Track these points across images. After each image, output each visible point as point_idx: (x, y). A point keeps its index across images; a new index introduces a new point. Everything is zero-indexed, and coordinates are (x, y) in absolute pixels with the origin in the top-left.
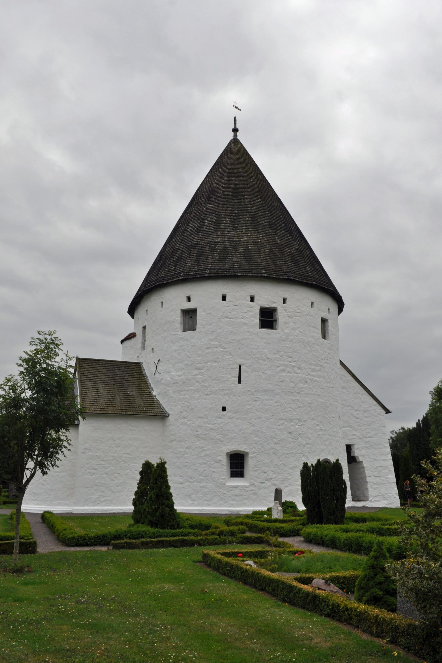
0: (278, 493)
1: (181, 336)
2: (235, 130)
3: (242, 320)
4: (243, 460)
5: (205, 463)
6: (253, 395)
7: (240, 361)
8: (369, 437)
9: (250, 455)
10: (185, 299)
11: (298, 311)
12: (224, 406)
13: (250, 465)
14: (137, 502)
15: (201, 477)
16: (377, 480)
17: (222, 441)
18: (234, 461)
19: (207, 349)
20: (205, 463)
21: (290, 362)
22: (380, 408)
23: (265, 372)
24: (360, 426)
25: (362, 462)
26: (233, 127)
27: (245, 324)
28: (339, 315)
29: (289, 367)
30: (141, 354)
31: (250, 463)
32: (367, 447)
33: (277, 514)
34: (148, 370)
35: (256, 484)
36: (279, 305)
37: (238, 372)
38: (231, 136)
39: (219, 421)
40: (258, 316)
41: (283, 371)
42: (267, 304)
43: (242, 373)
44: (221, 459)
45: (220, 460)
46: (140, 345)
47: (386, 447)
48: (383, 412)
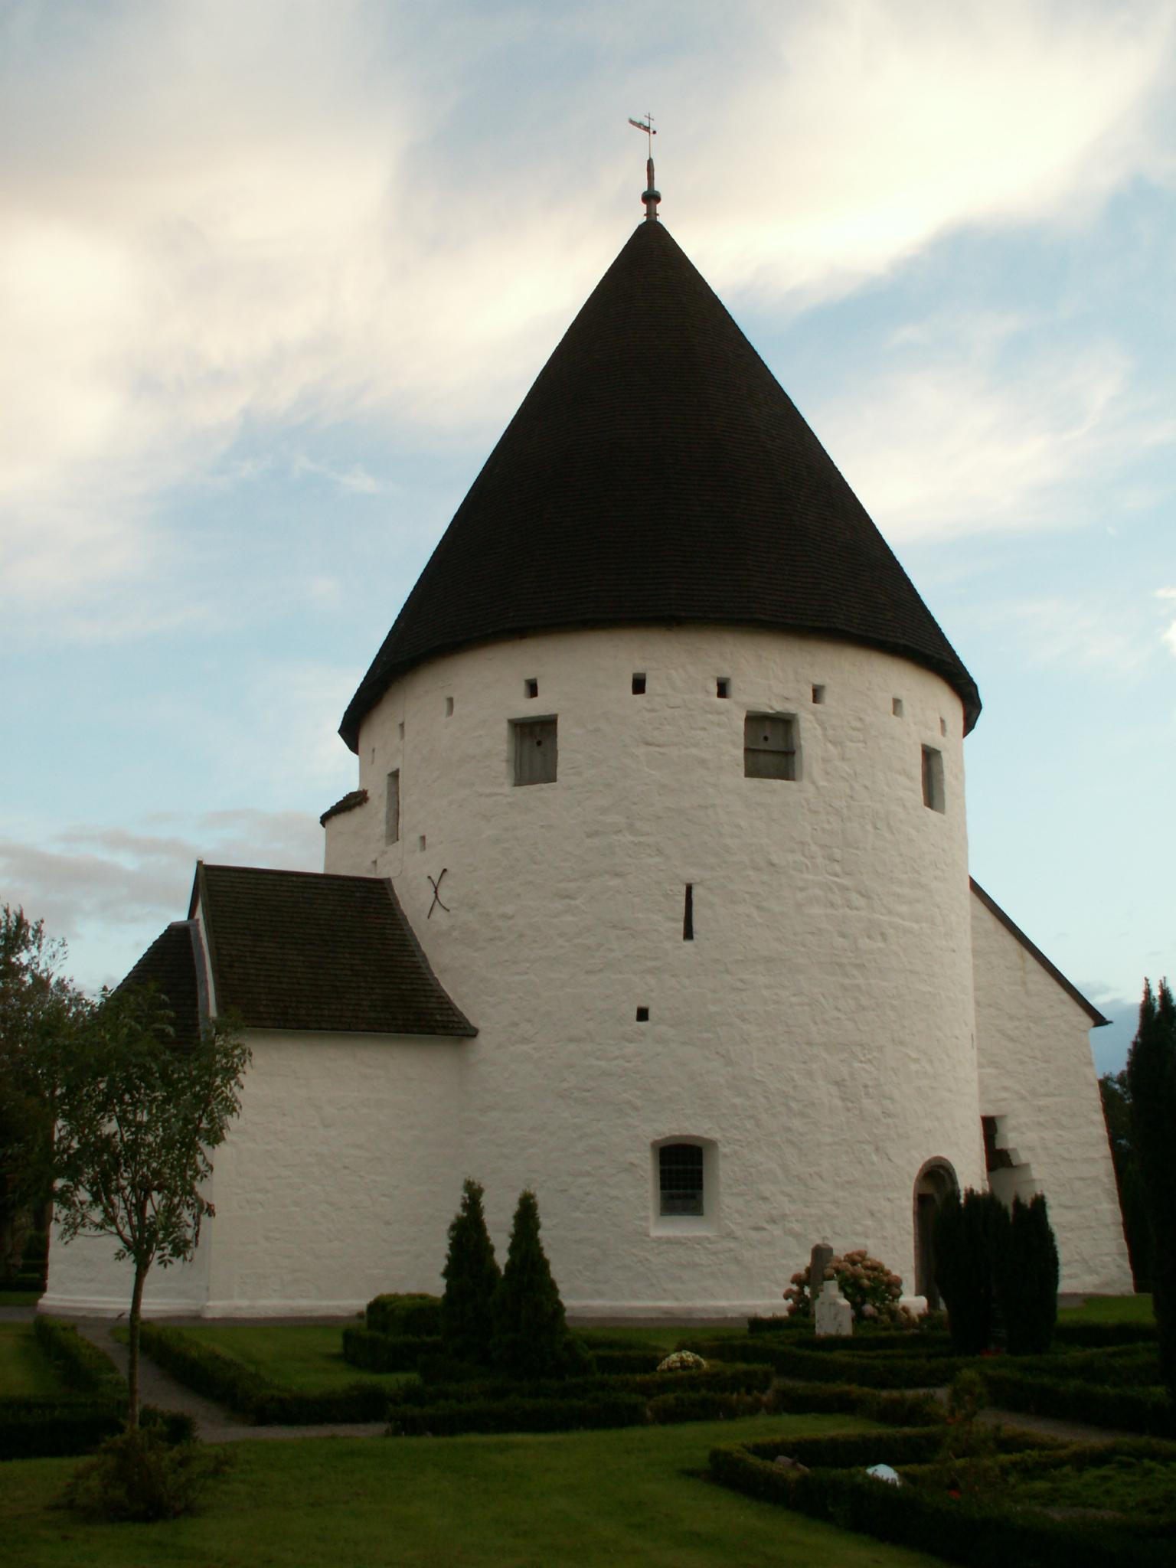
1: (510, 800)
2: (651, 198)
3: (694, 751)
4: (700, 1163)
5: (589, 1174)
6: (727, 971)
8: (1047, 1095)
9: (724, 1149)
10: (522, 688)
11: (858, 725)
12: (643, 1005)
13: (723, 1178)
14: (450, 1274)
15: (578, 1214)
17: (636, 1109)
18: (674, 1167)
19: (589, 836)
20: (589, 1174)
21: (836, 875)
22: (1080, 1011)
23: (764, 904)
24: (1022, 1062)
25: (1027, 1165)
27: (703, 762)
28: (965, 734)
29: (831, 889)
30: (384, 853)
31: (721, 1173)
32: (1040, 1124)
34: (413, 900)
35: (739, 1233)
37: (684, 904)
38: (637, 216)
39: (630, 1049)
43: (695, 908)
44: (636, 1162)
45: (632, 1164)
46: (381, 828)
47: (1093, 1123)
48: (1087, 1021)
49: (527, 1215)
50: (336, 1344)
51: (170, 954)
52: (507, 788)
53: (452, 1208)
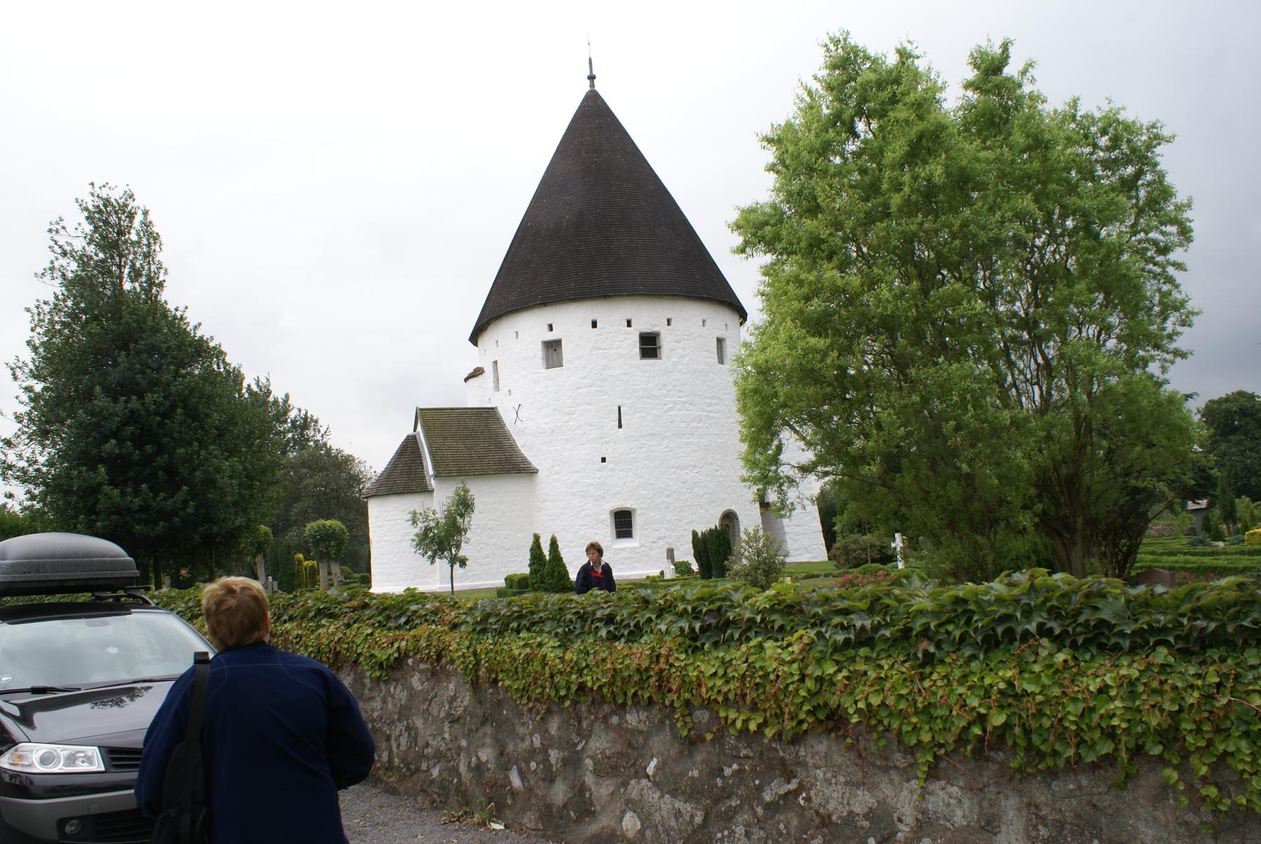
0: (670, 553)
2: (592, 78)
7: (619, 402)
9: (638, 512)
10: (546, 328)
13: (638, 523)
16: (798, 529)
26: (588, 73)
33: (670, 574)
34: (507, 417)
36: (661, 328)
40: (638, 345)
41: (672, 409)
42: (647, 328)
46: (491, 384)
49: (554, 544)
50: (495, 594)
51: (409, 448)
52: (544, 370)
53: (530, 542)
